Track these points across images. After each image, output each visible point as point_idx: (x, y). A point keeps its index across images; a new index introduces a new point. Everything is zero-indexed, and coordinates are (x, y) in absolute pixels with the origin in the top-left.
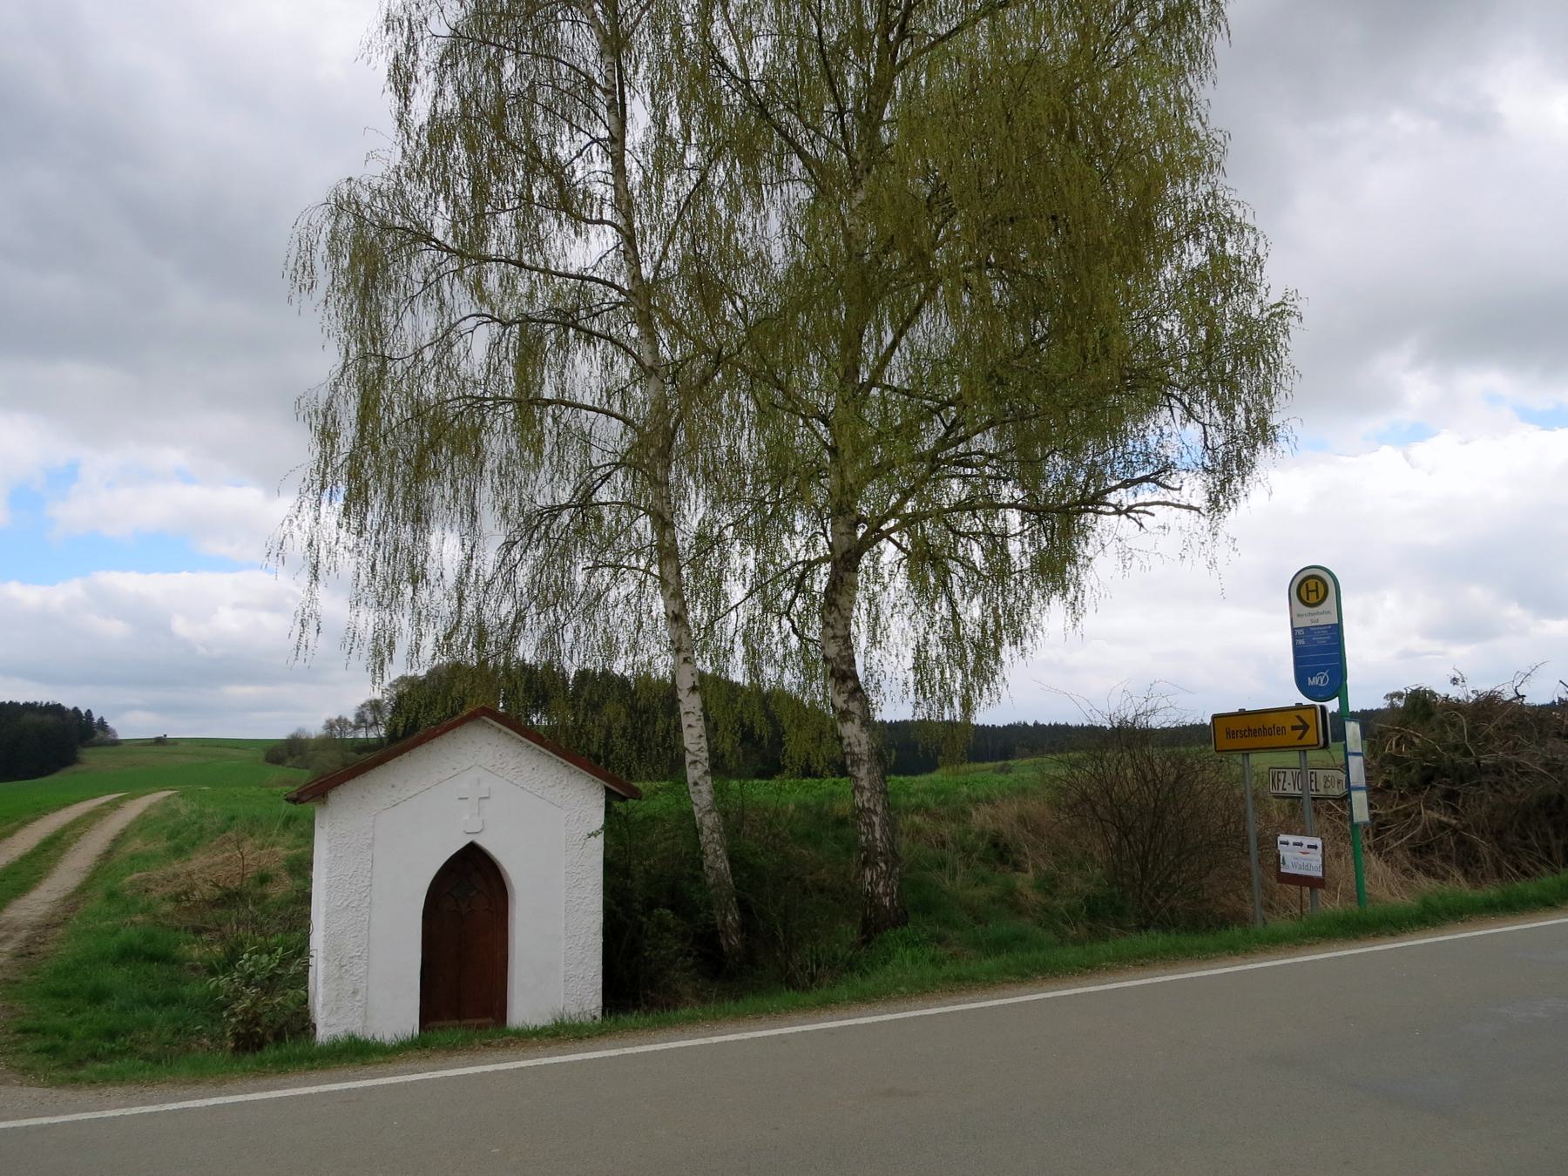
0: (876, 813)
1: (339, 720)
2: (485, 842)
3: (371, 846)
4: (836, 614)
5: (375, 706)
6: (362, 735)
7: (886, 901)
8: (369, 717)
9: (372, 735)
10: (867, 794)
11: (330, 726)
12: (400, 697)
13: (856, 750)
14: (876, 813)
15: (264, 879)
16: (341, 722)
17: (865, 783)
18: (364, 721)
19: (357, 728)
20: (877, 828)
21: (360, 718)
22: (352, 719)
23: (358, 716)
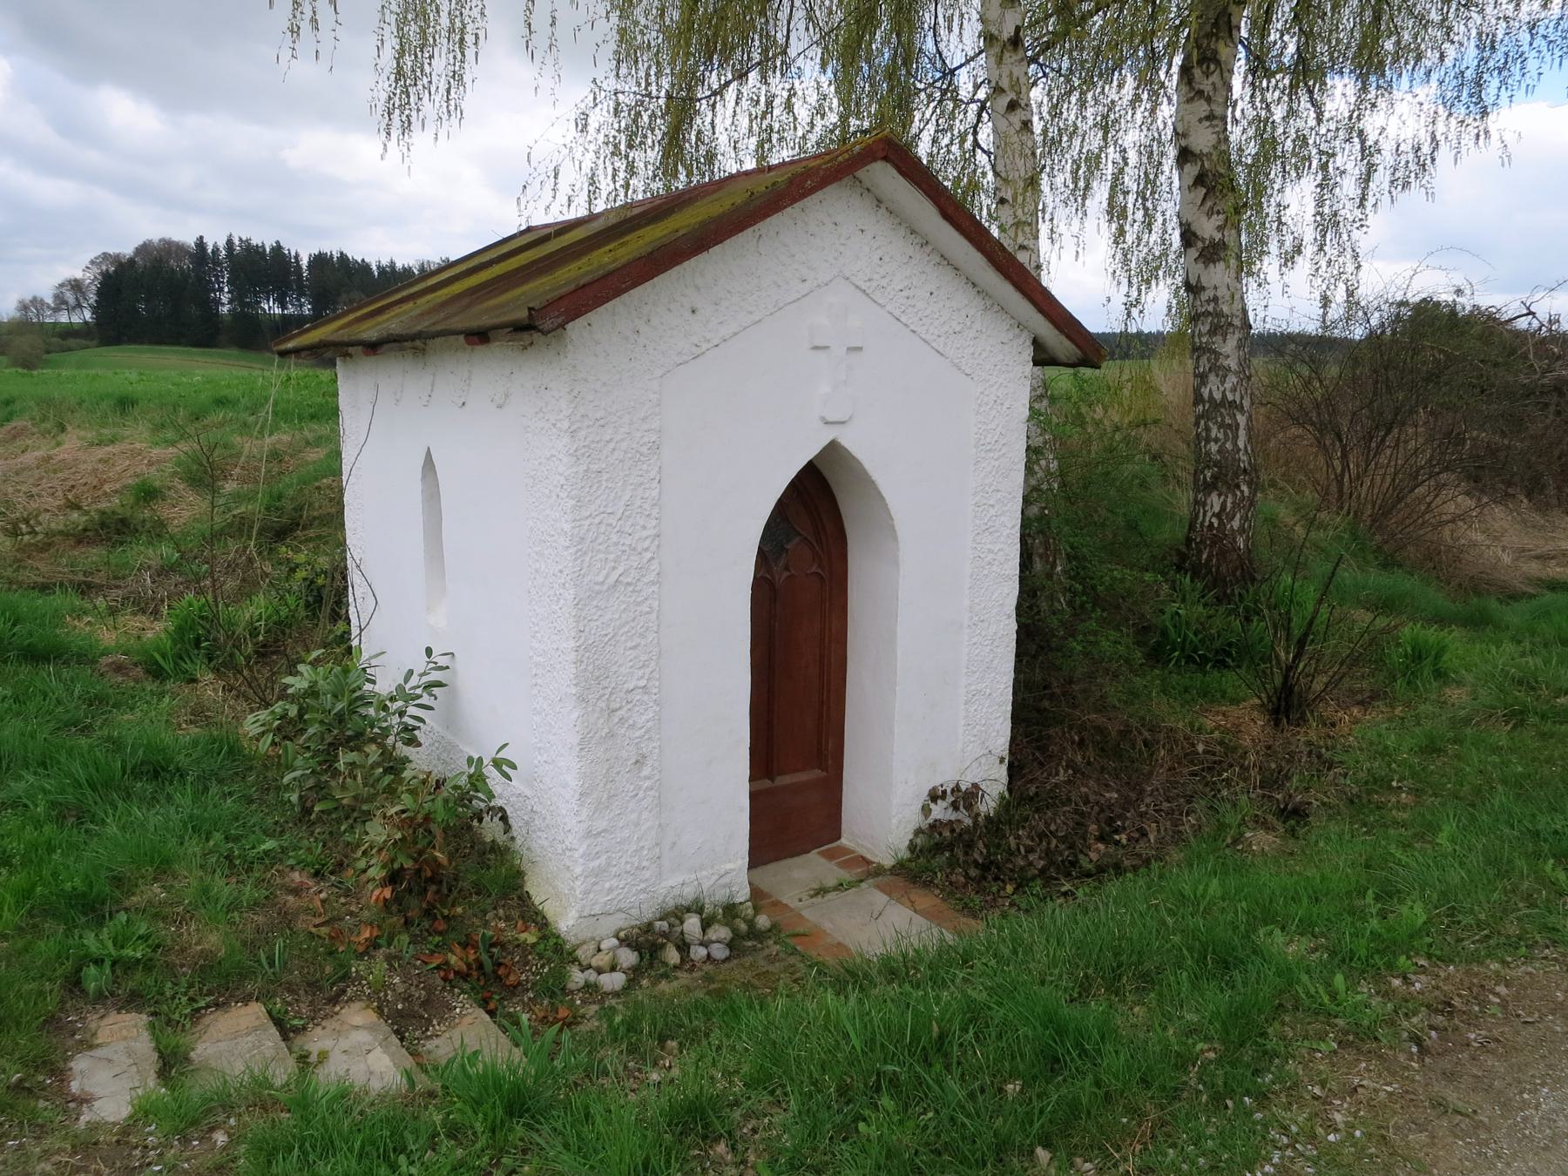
0: (1241, 408)
1: (34, 300)
2: (851, 441)
3: (656, 447)
4: (1215, 78)
5: (76, 286)
6: (63, 318)
7: (1241, 542)
8: (70, 297)
9: (76, 319)
10: (1232, 380)
11: (24, 307)
12: (106, 276)
13: (1225, 309)
14: (1241, 408)
15: (148, 494)
16: (37, 302)
17: (1232, 363)
18: (66, 303)
19: (56, 310)
20: (1242, 433)
21: (60, 302)
22: (50, 301)
23: (56, 297)
